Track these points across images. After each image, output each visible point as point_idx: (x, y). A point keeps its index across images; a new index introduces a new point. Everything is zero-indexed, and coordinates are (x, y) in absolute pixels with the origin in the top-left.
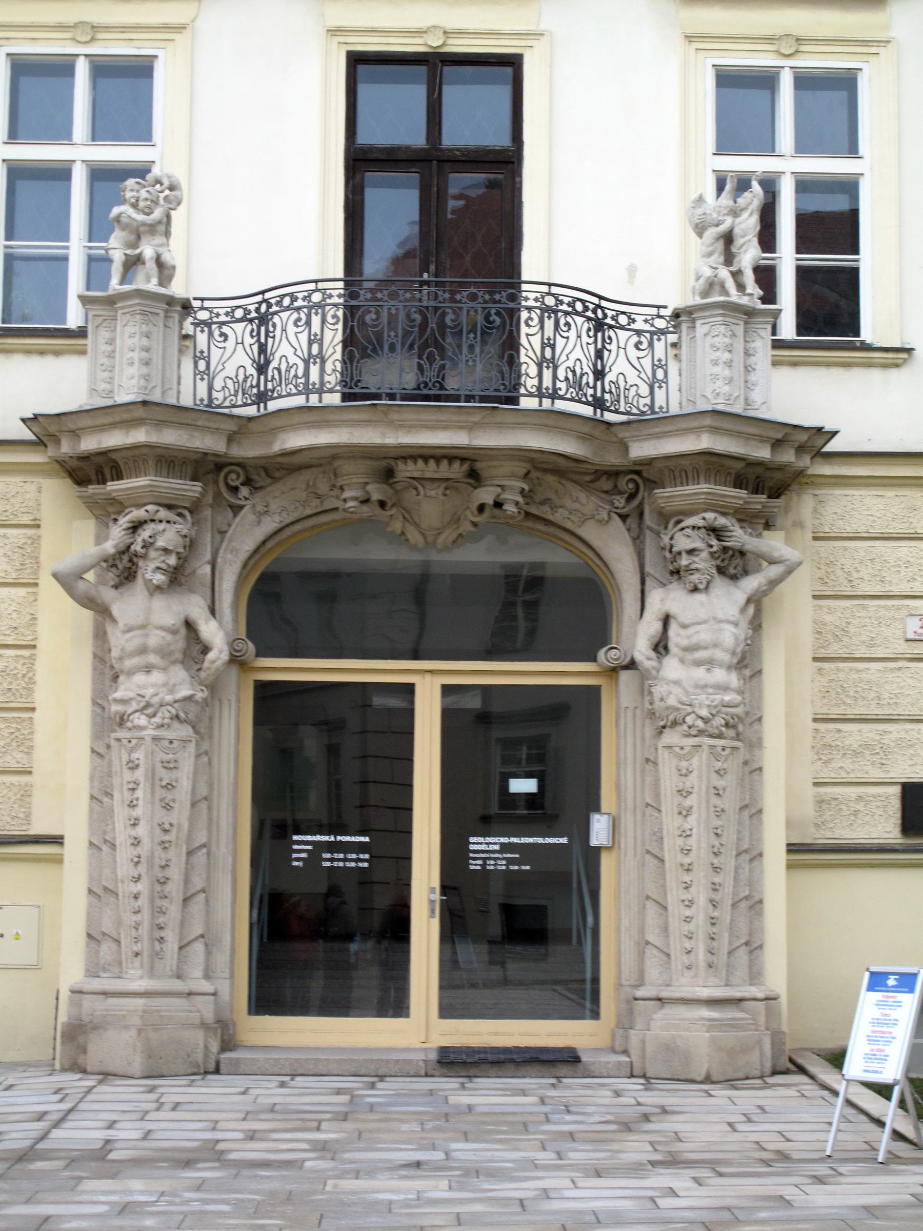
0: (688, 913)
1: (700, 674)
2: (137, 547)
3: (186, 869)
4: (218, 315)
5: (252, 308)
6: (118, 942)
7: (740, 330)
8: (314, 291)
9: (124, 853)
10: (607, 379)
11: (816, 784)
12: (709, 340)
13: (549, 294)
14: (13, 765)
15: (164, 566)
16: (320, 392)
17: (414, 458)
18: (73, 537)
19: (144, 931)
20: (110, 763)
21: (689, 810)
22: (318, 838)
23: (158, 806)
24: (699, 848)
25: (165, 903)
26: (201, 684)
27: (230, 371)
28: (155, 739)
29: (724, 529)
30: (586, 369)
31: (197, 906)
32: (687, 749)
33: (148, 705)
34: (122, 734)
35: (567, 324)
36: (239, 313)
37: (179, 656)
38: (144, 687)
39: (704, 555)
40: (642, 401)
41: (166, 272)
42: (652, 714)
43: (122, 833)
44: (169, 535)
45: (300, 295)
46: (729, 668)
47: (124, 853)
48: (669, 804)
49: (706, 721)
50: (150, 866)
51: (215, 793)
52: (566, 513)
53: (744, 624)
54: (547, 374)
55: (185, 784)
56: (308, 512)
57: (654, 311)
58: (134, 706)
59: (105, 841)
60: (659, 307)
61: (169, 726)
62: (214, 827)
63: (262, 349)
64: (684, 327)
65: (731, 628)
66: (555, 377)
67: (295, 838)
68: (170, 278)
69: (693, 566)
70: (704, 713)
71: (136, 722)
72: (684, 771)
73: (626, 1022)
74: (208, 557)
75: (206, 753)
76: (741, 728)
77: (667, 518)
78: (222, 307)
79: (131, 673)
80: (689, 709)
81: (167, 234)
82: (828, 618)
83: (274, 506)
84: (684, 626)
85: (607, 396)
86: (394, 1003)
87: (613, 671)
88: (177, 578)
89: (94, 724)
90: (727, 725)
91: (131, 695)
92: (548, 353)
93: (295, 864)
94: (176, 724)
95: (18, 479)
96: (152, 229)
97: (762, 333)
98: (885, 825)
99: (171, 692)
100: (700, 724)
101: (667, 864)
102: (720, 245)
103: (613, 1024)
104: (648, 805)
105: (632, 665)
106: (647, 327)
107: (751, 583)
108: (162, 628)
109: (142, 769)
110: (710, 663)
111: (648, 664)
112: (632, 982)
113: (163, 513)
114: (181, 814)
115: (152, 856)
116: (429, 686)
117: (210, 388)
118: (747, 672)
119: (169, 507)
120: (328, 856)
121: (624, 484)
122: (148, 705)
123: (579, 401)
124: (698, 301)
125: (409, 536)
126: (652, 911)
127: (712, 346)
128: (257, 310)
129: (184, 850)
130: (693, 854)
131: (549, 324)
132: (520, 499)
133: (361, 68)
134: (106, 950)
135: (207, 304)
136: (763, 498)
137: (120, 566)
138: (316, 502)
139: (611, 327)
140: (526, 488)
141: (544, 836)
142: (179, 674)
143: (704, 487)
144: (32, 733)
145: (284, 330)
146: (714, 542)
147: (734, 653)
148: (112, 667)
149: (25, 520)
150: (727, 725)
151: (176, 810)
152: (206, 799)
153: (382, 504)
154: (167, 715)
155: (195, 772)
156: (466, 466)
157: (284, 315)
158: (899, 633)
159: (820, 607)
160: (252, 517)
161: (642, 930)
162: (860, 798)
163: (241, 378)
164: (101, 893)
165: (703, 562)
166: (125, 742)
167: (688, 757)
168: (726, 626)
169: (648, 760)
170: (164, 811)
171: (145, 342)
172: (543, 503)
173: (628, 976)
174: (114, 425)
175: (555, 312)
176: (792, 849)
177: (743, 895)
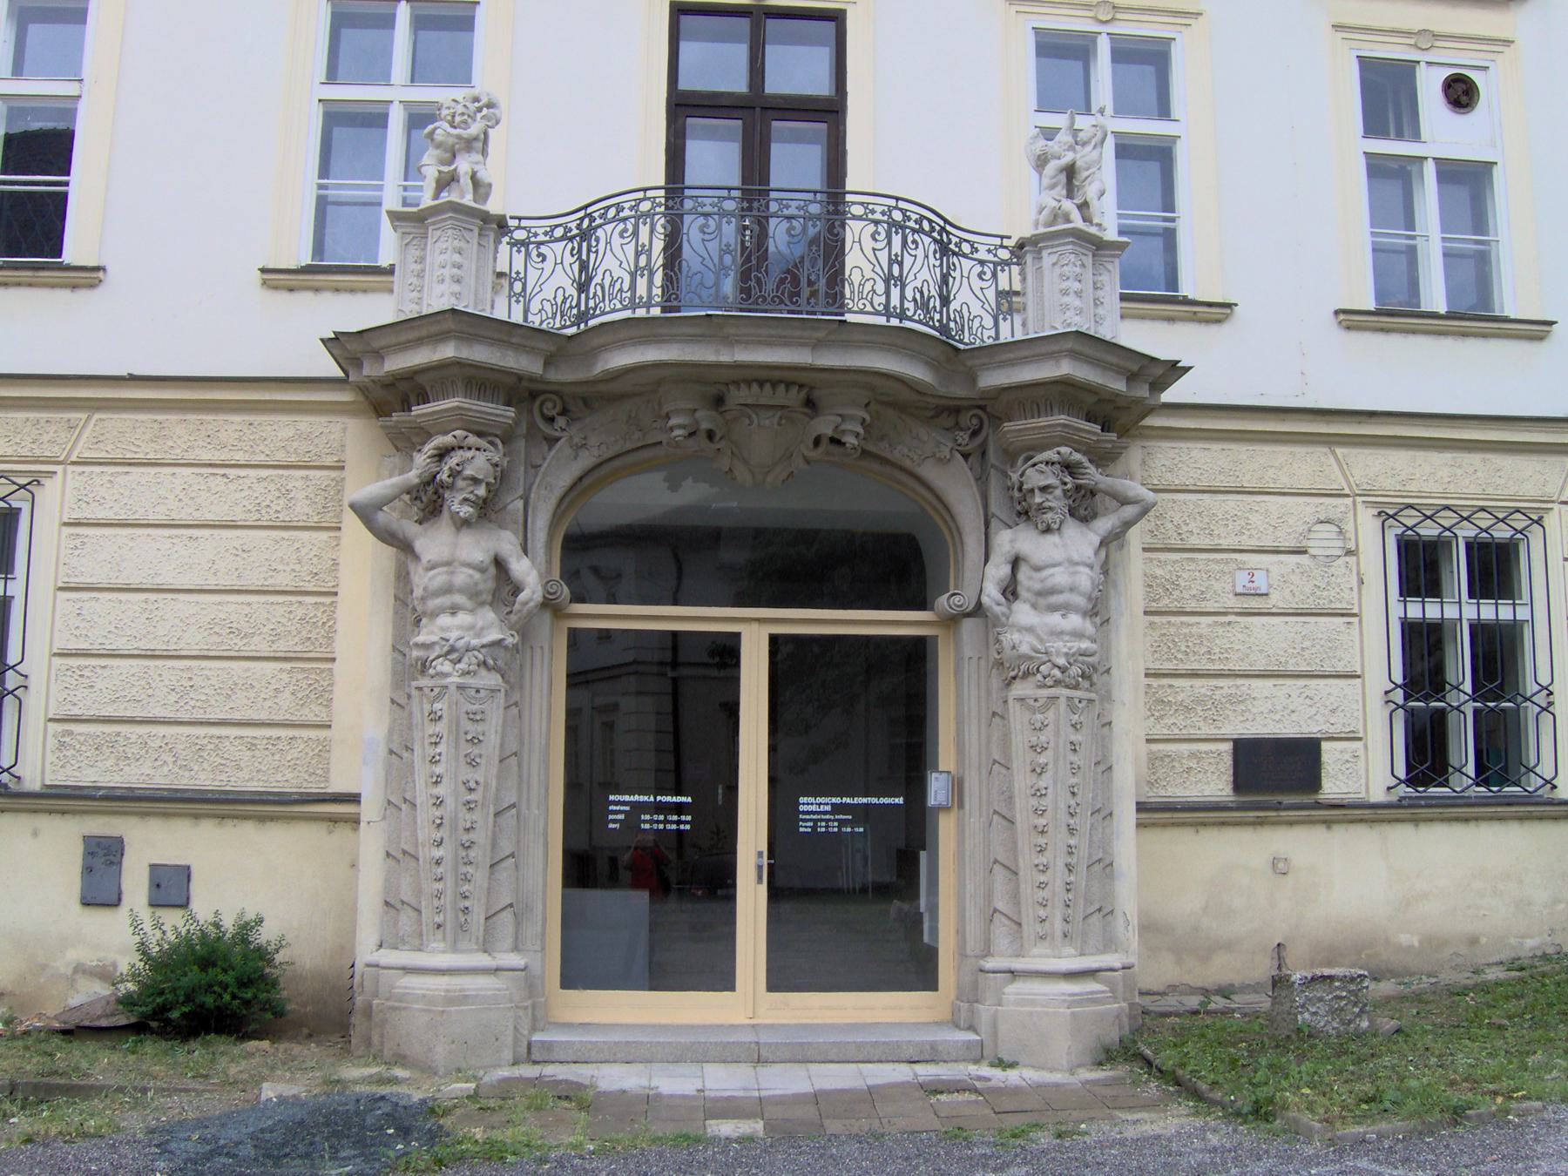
0: (1043, 878)
1: (1055, 619)
2: (444, 476)
3: (494, 833)
4: (536, 235)
5: (573, 226)
6: (419, 911)
7: (1089, 261)
8: (641, 200)
9: (425, 814)
10: (953, 306)
11: (1148, 741)
12: (1057, 270)
13: (896, 208)
14: (312, 718)
15: (472, 497)
16: (648, 306)
17: (749, 382)
18: (372, 473)
19: (447, 900)
20: (411, 714)
21: (1044, 767)
22: (636, 798)
23: (462, 760)
24: (1056, 808)
25: (470, 869)
26: (511, 628)
28: (461, 688)
29: (1079, 464)
30: (933, 293)
31: (505, 873)
32: (1041, 702)
33: (452, 650)
34: (424, 682)
35: (914, 242)
36: (559, 232)
37: (487, 597)
38: (448, 629)
39: (1058, 492)
40: (986, 334)
41: (482, 191)
42: (1000, 664)
43: (422, 792)
44: (479, 462)
45: (627, 205)
46: (1085, 614)
47: (425, 814)
48: (1021, 760)
49: (1063, 670)
50: (454, 828)
51: (526, 747)
52: (906, 451)
53: (1097, 568)
54: (895, 293)
55: (493, 739)
56: (629, 446)
57: (998, 241)
58: (437, 651)
59: (405, 800)
60: (1002, 237)
61: (475, 673)
62: (525, 786)
63: (584, 266)
64: (1029, 258)
65: (1087, 570)
66: (903, 297)
67: (612, 798)
68: (487, 196)
69: (1047, 504)
70: (1062, 661)
71: (439, 668)
72: (1038, 725)
73: (971, 994)
74: (520, 492)
75: (516, 704)
76: (1095, 678)
77: (1011, 456)
78: (540, 227)
79: (434, 615)
80: (1045, 658)
81: (484, 152)
82: (1159, 572)
83: (593, 441)
84: (1038, 569)
85: (952, 325)
86: (723, 979)
87: (952, 621)
88: (487, 511)
89: (394, 673)
90: (1083, 676)
91: (435, 638)
92: (896, 272)
93: (611, 826)
94: (483, 672)
95: (323, 419)
96: (469, 144)
97: (1109, 266)
98: (1216, 784)
99: (478, 635)
100: (1056, 672)
101: (1018, 825)
102: (1063, 178)
103: (953, 996)
104: (995, 762)
105: (978, 610)
106: (990, 257)
107: (1104, 524)
108: (469, 565)
109: (445, 720)
110: (1065, 609)
111: (997, 609)
112: (978, 952)
113: (473, 440)
114: (487, 773)
115: (455, 819)
116: (755, 632)
117: (526, 311)
118: (1098, 620)
119: (480, 434)
120: (648, 817)
121: (966, 419)
122: (452, 650)
123: (926, 324)
124: (1042, 230)
125: (736, 473)
126: (1000, 874)
127: (1061, 275)
128: (579, 227)
129: (492, 811)
130: (1049, 814)
131: (897, 240)
132: (861, 431)
133: (686, 20)
134: (406, 919)
135: (524, 223)
136: (1113, 436)
137: (425, 499)
138: (637, 435)
139: (954, 254)
140: (868, 418)
141: (852, 796)
142: (488, 615)
143: (1062, 419)
144: (331, 685)
145: (608, 243)
146: (1068, 479)
147: (1090, 599)
148: (414, 610)
149: (329, 461)
150: (1083, 676)
151: (483, 768)
152: (515, 754)
153: (710, 435)
154: (474, 661)
155: (504, 726)
156: (803, 393)
157: (609, 228)
158: (1229, 587)
159: (1151, 560)
160: (568, 451)
161: (989, 896)
162: (1192, 755)
163: (560, 299)
164: (399, 856)
165: (1057, 501)
166: (427, 691)
167: (1044, 709)
168: (1081, 569)
169: (994, 714)
170: (469, 769)
171: (457, 258)
172: (882, 438)
173: (972, 946)
174: (419, 342)
175: (903, 228)
176: (1141, 807)
177: (1095, 858)
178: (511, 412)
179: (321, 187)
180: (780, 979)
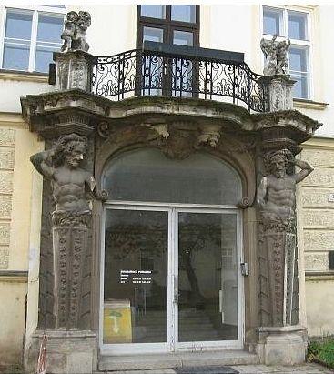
27: (105, 82)
63: (121, 73)
88: (81, 165)
163: (110, 84)
178: (92, 128)
179: (5, 40)
180: (183, 337)
